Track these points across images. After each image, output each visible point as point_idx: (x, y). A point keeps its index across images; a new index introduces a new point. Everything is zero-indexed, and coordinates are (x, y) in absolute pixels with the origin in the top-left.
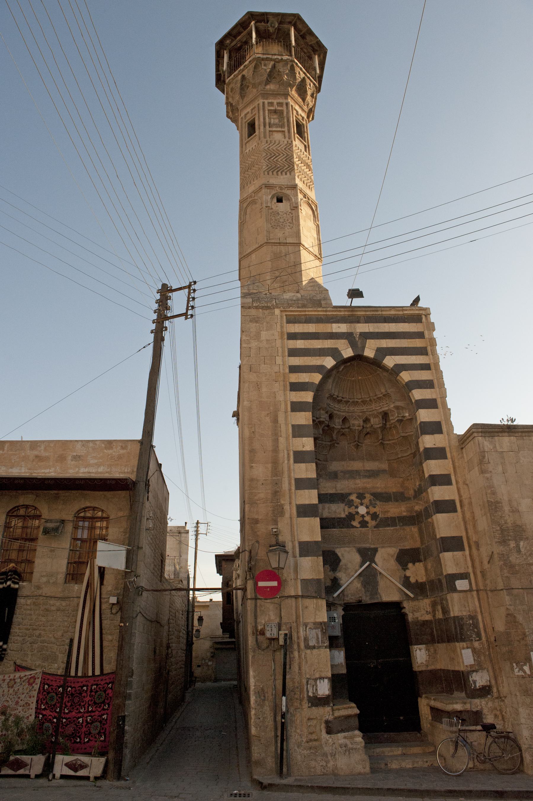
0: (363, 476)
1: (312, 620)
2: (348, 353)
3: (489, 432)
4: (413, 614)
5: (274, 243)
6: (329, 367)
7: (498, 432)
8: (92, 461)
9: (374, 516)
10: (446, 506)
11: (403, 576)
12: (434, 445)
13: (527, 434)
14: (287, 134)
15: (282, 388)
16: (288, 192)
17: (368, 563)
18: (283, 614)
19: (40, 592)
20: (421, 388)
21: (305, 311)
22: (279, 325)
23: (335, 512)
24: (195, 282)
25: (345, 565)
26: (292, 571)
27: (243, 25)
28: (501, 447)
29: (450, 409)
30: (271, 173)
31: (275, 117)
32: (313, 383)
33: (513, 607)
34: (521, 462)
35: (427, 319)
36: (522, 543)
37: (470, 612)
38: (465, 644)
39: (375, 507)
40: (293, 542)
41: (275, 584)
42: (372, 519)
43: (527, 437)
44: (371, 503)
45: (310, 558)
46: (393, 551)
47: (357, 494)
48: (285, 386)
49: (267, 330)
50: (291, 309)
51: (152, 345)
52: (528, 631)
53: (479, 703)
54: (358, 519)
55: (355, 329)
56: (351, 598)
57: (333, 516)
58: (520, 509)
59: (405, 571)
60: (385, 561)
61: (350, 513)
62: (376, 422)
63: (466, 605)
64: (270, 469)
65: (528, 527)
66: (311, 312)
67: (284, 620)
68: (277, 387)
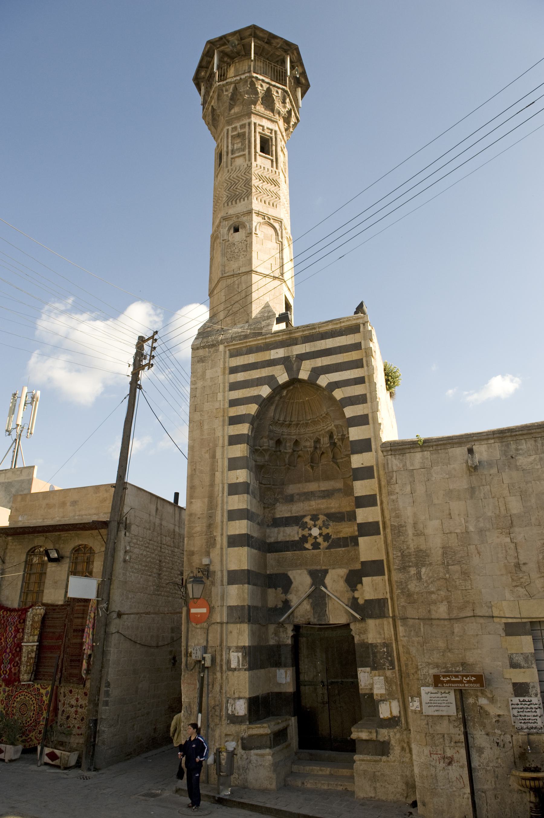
1: (235, 644)
2: (283, 378)
3: (400, 449)
4: (360, 636)
5: (228, 276)
6: (265, 396)
7: (409, 448)
9: (327, 537)
10: (370, 529)
11: (351, 598)
12: (362, 464)
13: (442, 447)
15: (221, 424)
18: (209, 638)
20: (353, 405)
21: (247, 342)
22: (222, 361)
23: (289, 535)
25: (297, 588)
26: (219, 598)
27: (208, 55)
28: (412, 464)
29: (380, 424)
31: (238, 141)
32: (249, 414)
33: (406, 638)
34: (433, 479)
35: (364, 328)
36: (423, 570)
37: (384, 639)
38: (377, 672)
39: (327, 528)
40: (222, 571)
41: (204, 610)
42: (324, 541)
43: (443, 451)
44: (324, 525)
45: (237, 586)
46: (343, 572)
47: (311, 515)
48: (224, 421)
49: (212, 368)
50: (234, 342)
52: (421, 665)
53: (386, 733)
54: (311, 541)
55: (292, 351)
56: (299, 619)
57: (288, 540)
58: (426, 531)
59: (354, 592)
60: (335, 581)
61: (303, 536)
62: (325, 441)
63: (382, 632)
64: (206, 502)
65: (433, 551)
66: (252, 342)
67: (211, 643)
68: (217, 423)
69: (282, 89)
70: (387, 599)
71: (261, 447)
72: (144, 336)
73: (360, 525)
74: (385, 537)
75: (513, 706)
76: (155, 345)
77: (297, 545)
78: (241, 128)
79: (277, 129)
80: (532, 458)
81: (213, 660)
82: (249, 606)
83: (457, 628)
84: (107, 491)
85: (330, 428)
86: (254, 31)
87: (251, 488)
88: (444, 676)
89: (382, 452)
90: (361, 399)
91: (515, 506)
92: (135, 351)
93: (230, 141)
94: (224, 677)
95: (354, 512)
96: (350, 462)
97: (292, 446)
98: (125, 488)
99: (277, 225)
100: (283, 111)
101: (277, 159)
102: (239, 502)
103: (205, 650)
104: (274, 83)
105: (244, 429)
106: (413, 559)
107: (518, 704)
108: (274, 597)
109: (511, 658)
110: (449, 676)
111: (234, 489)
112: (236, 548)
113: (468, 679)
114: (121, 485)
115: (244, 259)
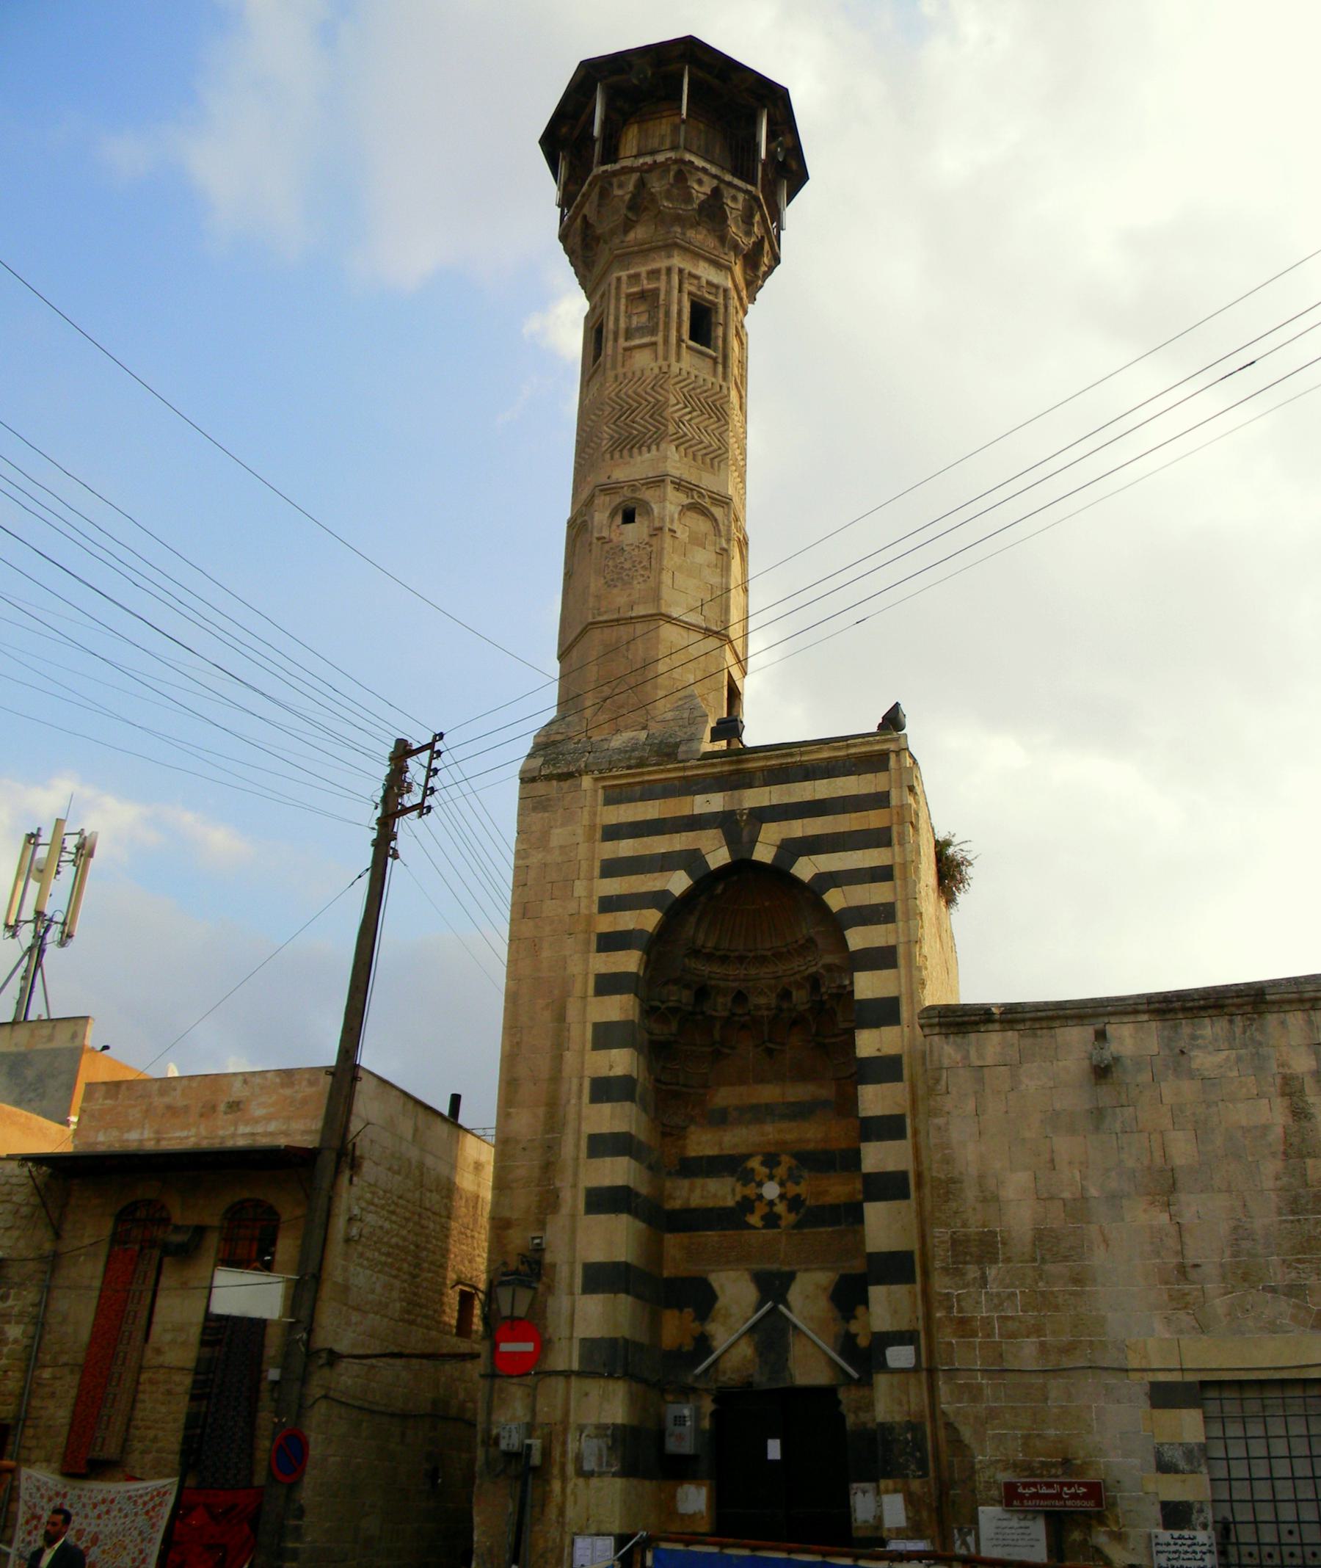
0: (752, 1121)
1: (593, 1420)
2: (718, 857)
5: (606, 622)
8: (259, 1112)
9: (794, 1203)
10: (890, 1186)
13: (1044, 1024)
14: (660, 348)
16: (648, 495)
17: (769, 1305)
19: (161, 1359)
24: (441, 735)
28: (981, 1056)
30: (617, 455)
32: (642, 931)
35: (898, 761)
39: (797, 1183)
41: (529, 1347)
42: (790, 1210)
48: (588, 942)
49: (563, 825)
51: (367, 876)
54: (761, 1209)
55: (740, 801)
57: (711, 1205)
59: (848, 1322)
60: (807, 1299)
61: (745, 1198)
69: (746, 192)
70: (918, 1332)
71: (663, 1002)
72: (410, 741)
73: (868, 1178)
74: (920, 1204)
75: (1160, 1548)
76: (435, 764)
77: (731, 1218)
78: (648, 278)
79: (730, 285)
80: (1223, 1055)
81: (546, 1453)
82: (626, 1340)
83: (1056, 1387)
84: (311, 1083)
85: (814, 969)
86: (690, 53)
87: (639, 1089)
88: (1026, 1485)
89: (922, 1027)
90: (883, 914)
91: (1182, 1149)
92: (388, 770)
93: (623, 308)
94: (569, 1490)
95: (857, 1153)
96: (852, 1044)
97: (729, 1004)
98: (355, 1078)
99: (718, 512)
100: (746, 242)
101: (725, 357)
102: (611, 1118)
103: (530, 1429)
104: (728, 178)
105: (630, 962)
106: (974, 1249)
107: (1168, 1544)
108: (675, 1328)
109: (1159, 1455)
110: (1034, 1485)
111: (604, 1090)
112: (602, 1216)
113: (1073, 1490)
114: (346, 1071)
115: (642, 586)
